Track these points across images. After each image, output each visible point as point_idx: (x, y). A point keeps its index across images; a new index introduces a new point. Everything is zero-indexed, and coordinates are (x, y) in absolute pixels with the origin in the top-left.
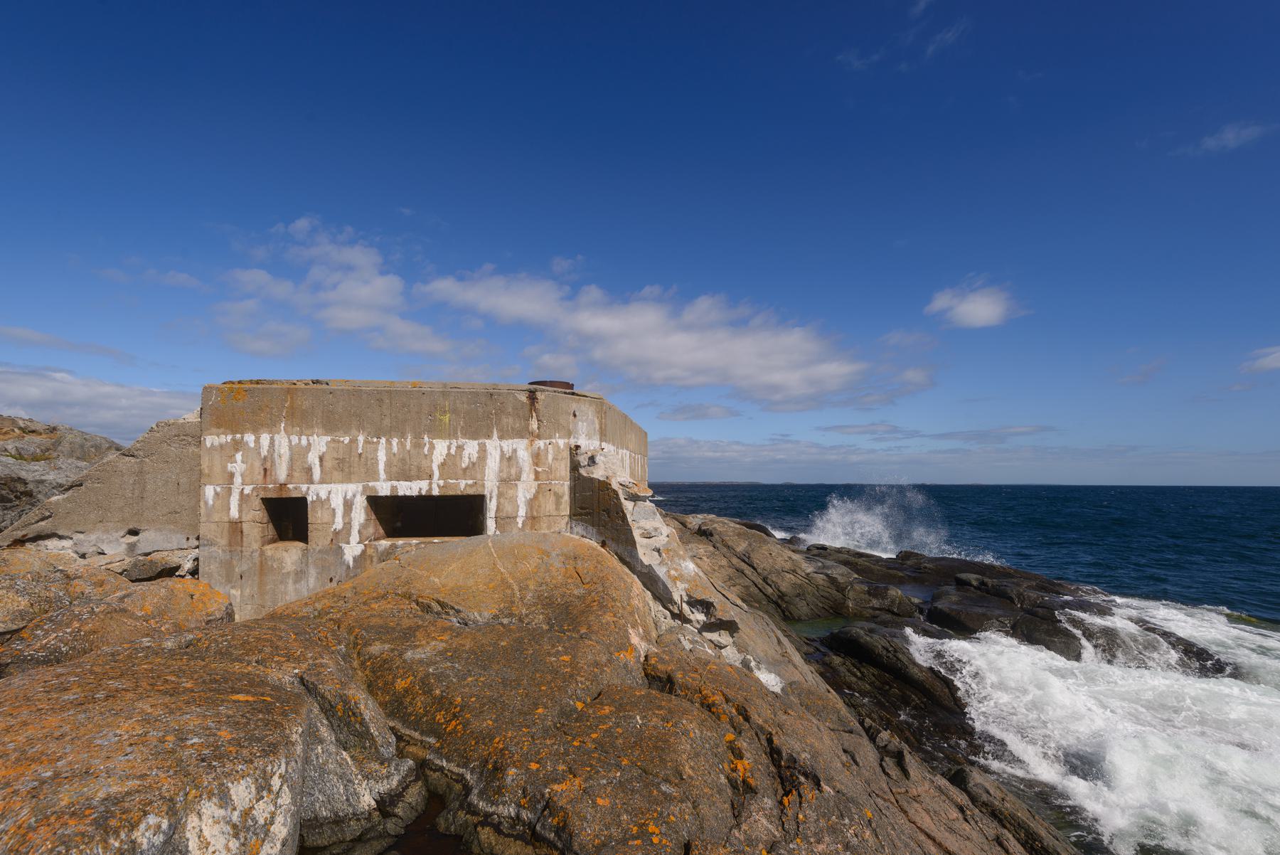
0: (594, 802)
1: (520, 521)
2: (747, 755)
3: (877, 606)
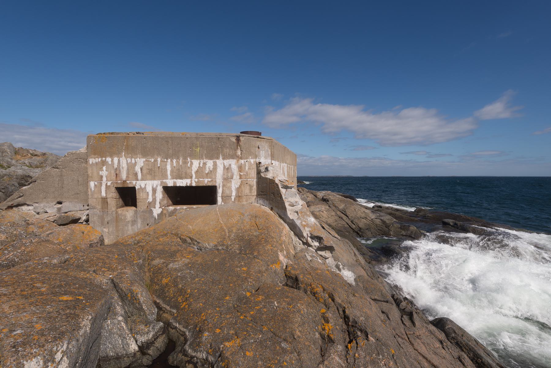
0: (245, 354)
1: (233, 198)
2: (331, 321)
3: (405, 234)
